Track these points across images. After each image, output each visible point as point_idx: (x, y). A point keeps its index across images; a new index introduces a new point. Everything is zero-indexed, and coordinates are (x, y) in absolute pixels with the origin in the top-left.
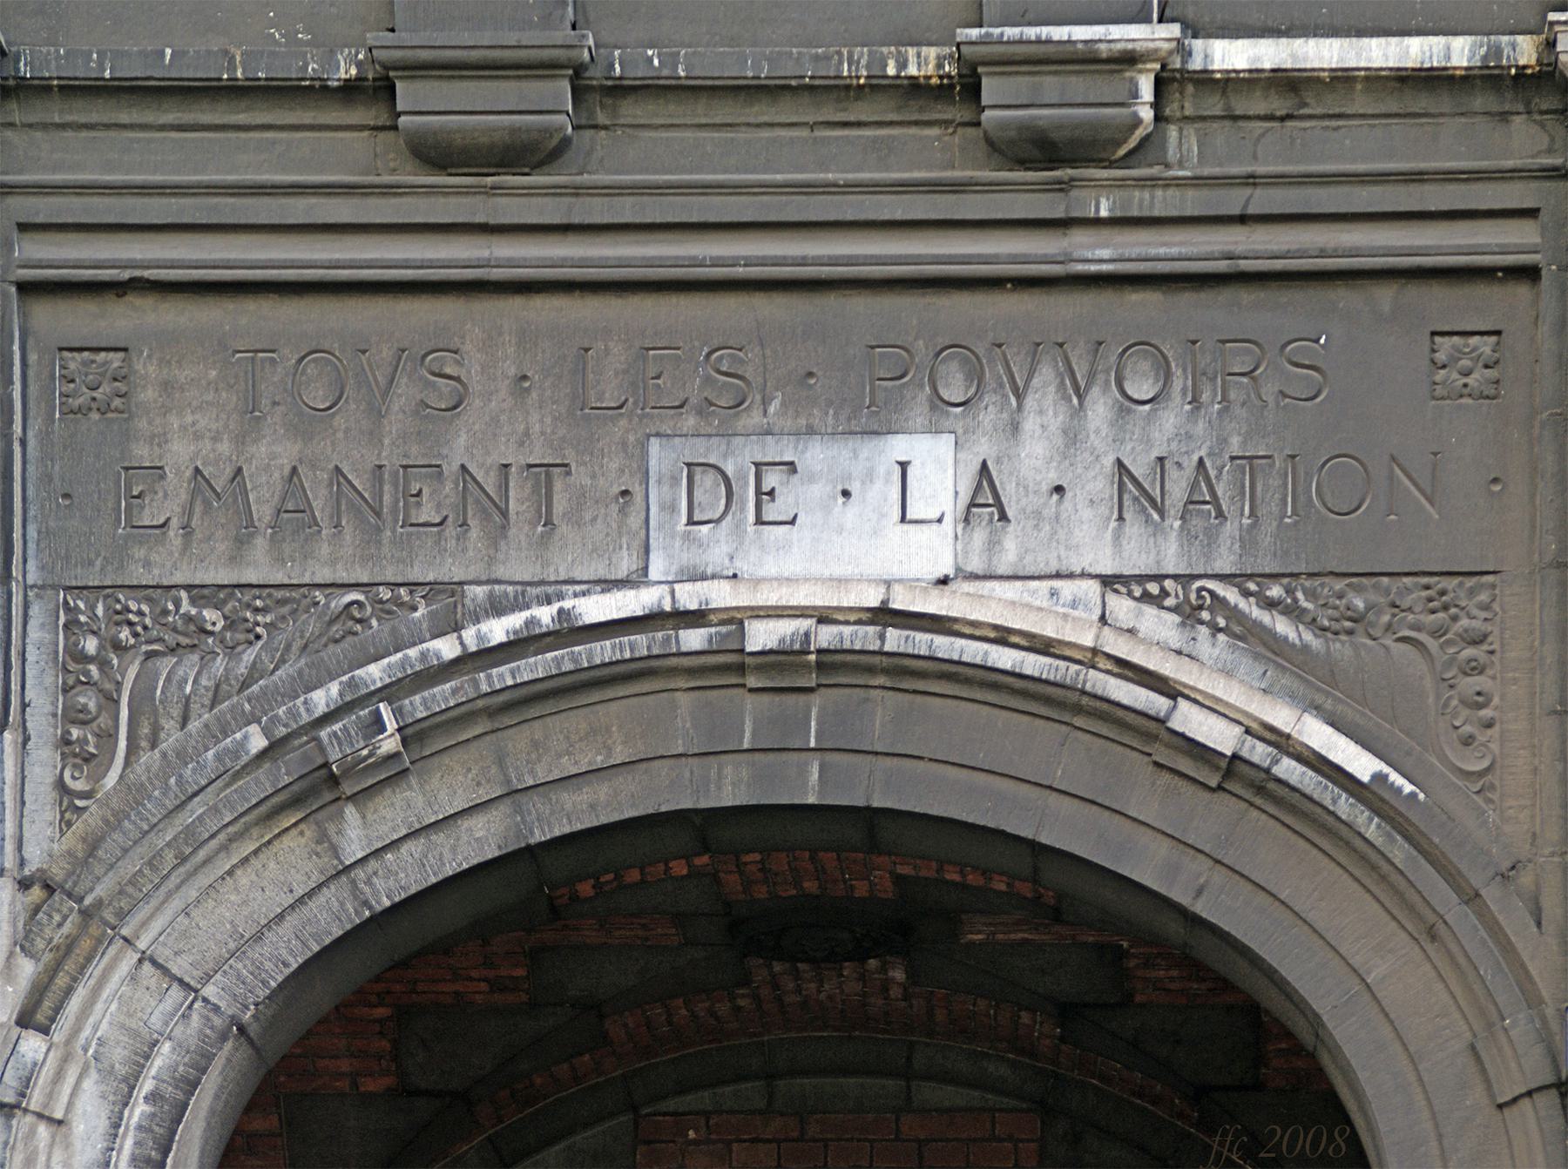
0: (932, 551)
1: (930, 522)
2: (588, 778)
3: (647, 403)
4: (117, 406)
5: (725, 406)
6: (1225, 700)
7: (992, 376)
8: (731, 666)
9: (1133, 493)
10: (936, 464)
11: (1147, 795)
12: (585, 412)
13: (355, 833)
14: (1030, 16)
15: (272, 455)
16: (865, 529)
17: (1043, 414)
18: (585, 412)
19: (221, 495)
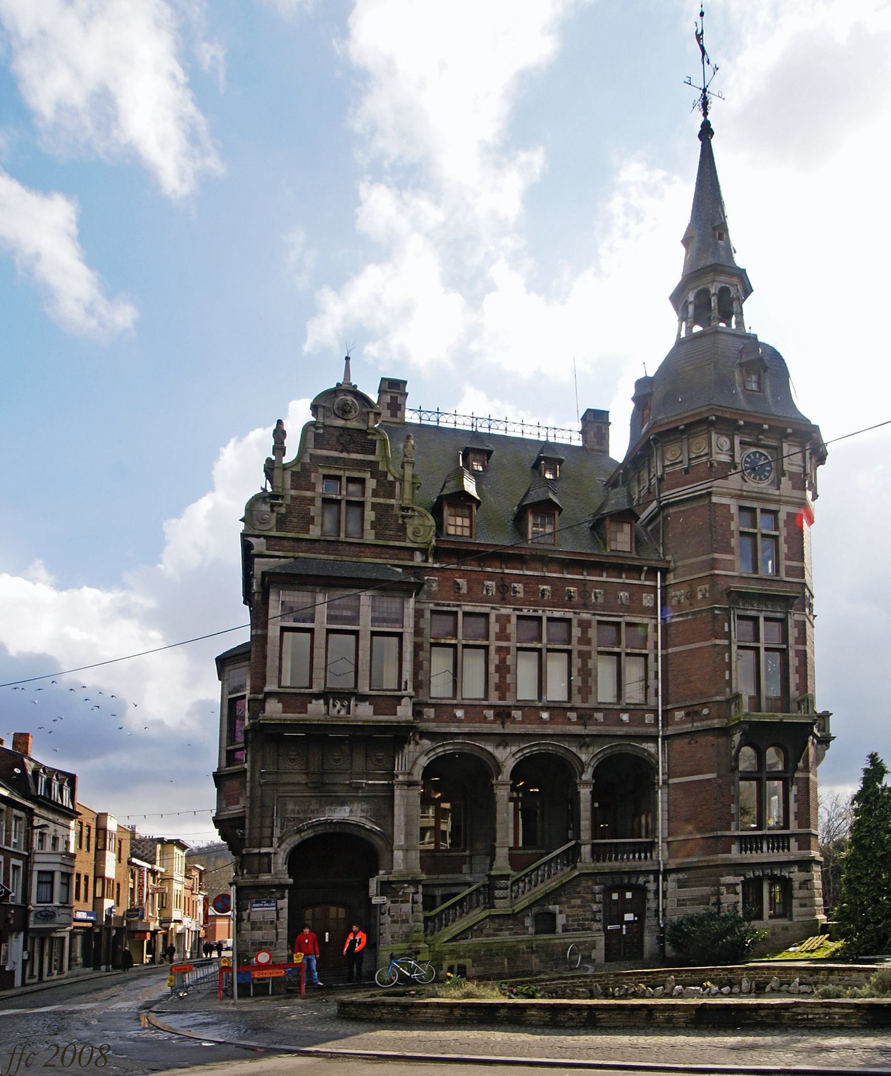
0: (347, 815)
1: (705, 114)
2: (320, 830)
3: (326, 804)
4: (285, 804)
5: (332, 804)
6: (369, 825)
7: (352, 802)
8: (332, 822)
9: (362, 811)
10: (347, 808)
11: (363, 831)
12: (321, 805)
13: (302, 834)
14: (645, 1012)
15: (297, 808)
16: (341, 814)
17: (356, 805)
18: (321, 805)
19: (293, 811)
